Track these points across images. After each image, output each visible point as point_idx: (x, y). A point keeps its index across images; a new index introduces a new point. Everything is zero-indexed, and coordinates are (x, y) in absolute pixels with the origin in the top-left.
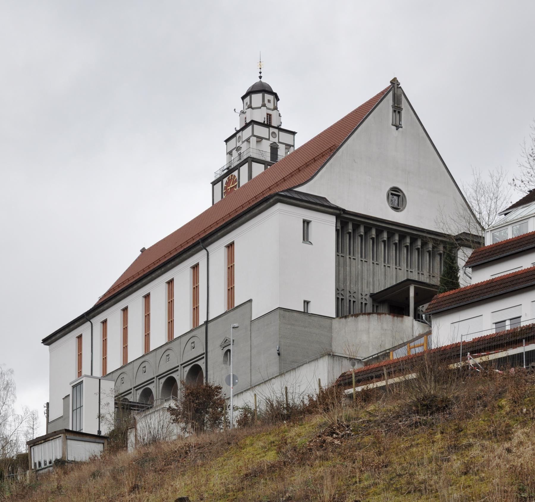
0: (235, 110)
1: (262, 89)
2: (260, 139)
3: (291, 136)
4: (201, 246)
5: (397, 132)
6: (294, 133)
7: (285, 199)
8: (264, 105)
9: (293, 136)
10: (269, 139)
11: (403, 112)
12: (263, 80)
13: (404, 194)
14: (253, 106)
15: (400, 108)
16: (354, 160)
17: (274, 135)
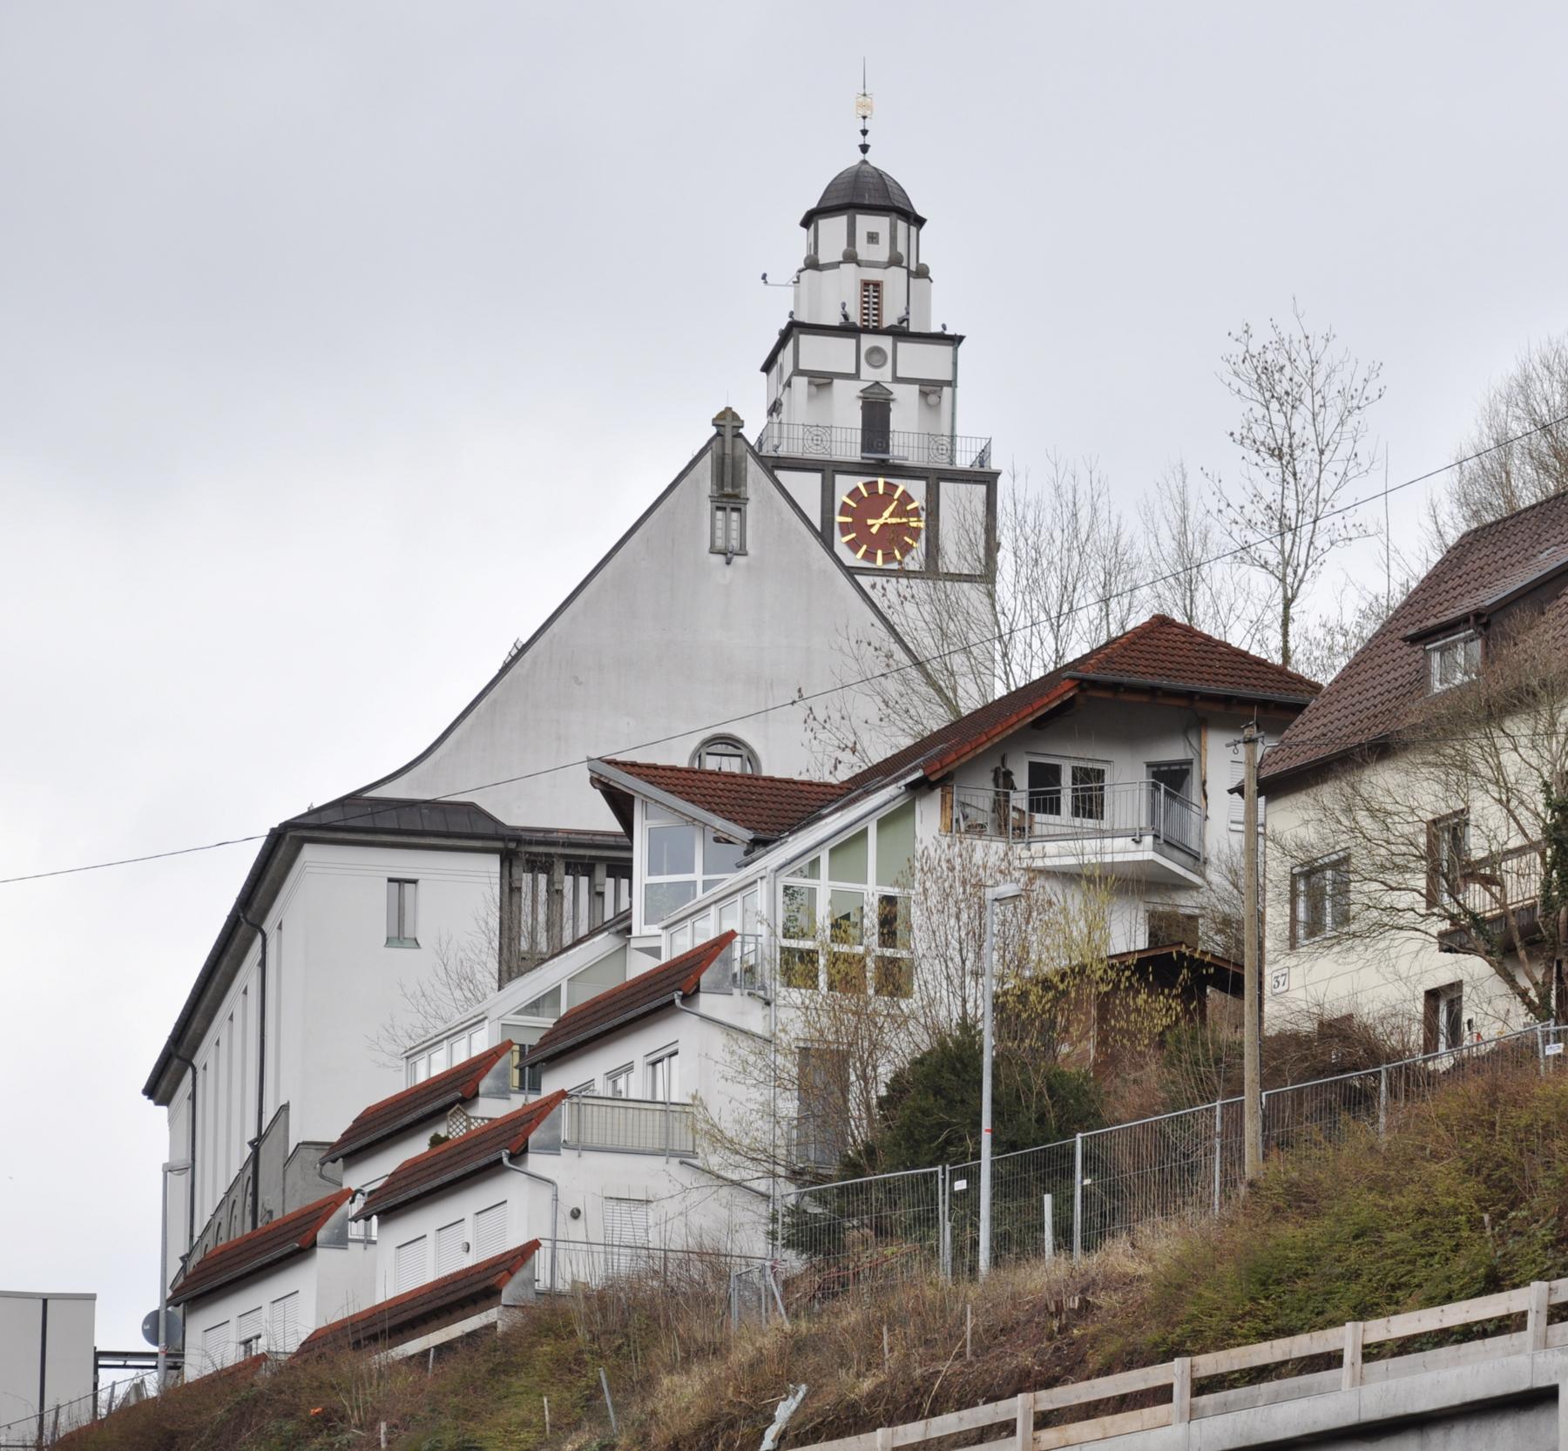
0: (764, 277)
1: (863, 196)
2: (822, 381)
3: (945, 351)
4: (243, 929)
5: (729, 570)
6: (956, 340)
7: (317, 834)
8: (850, 257)
9: (950, 349)
10: (856, 376)
11: (750, 509)
12: (874, 158)
13: (752, 752)
14: (823, 259)
15: (736, 496)
16: (576, 678)
17: (876, 357)
